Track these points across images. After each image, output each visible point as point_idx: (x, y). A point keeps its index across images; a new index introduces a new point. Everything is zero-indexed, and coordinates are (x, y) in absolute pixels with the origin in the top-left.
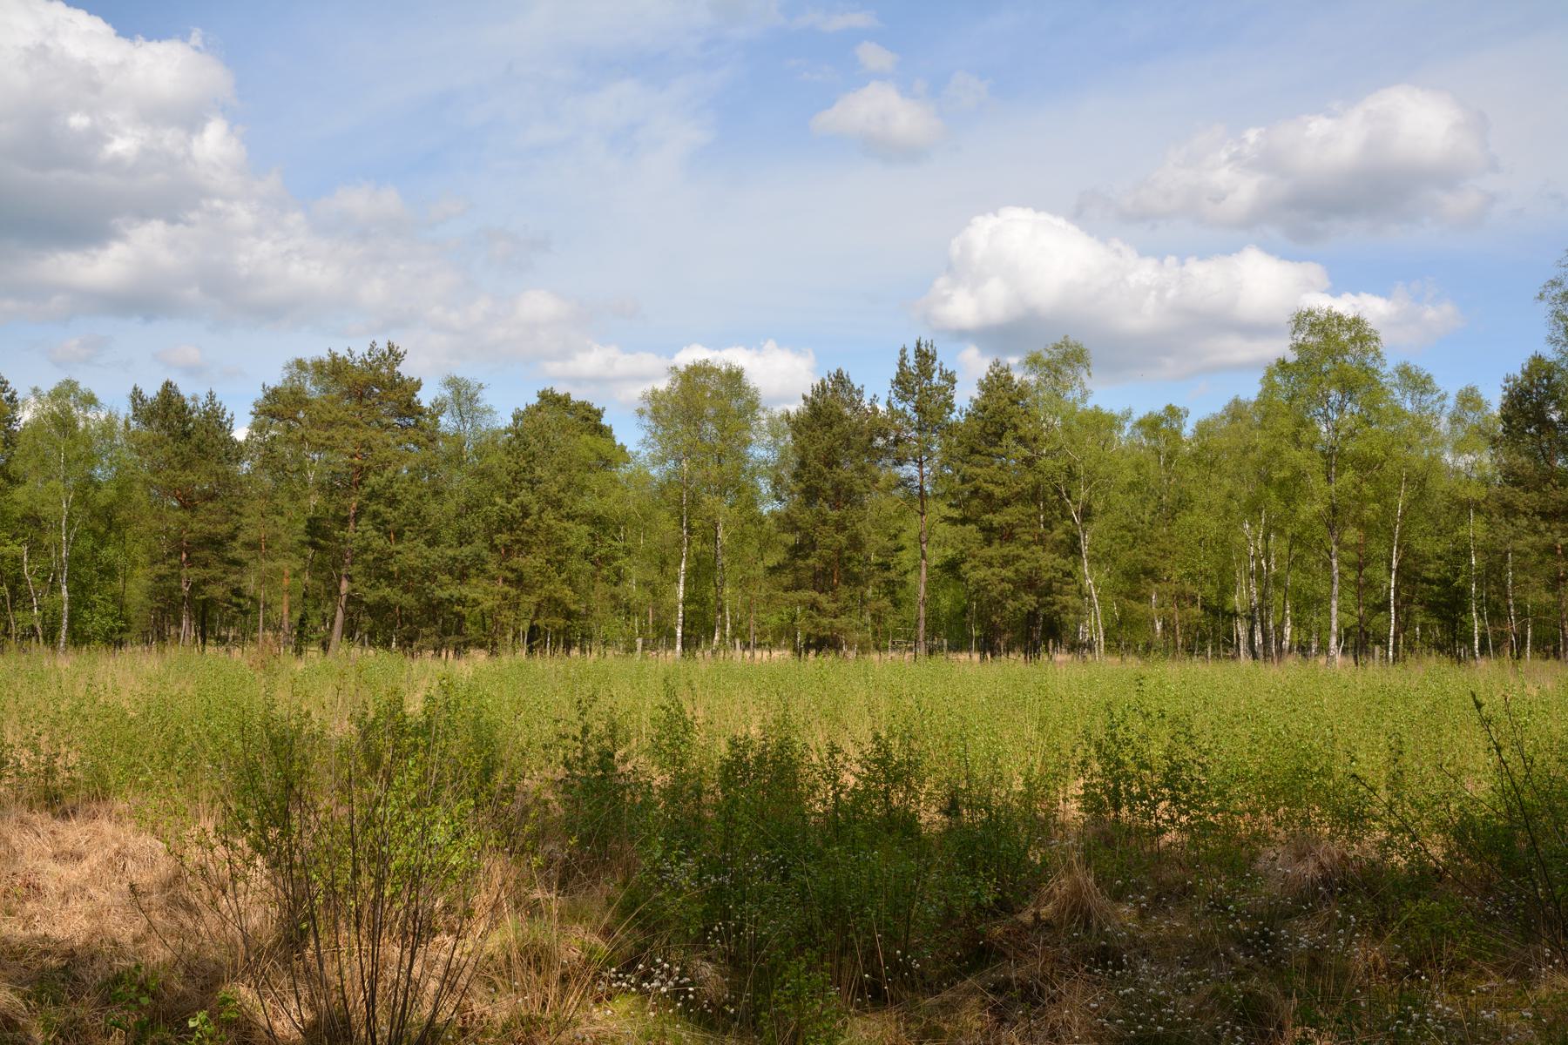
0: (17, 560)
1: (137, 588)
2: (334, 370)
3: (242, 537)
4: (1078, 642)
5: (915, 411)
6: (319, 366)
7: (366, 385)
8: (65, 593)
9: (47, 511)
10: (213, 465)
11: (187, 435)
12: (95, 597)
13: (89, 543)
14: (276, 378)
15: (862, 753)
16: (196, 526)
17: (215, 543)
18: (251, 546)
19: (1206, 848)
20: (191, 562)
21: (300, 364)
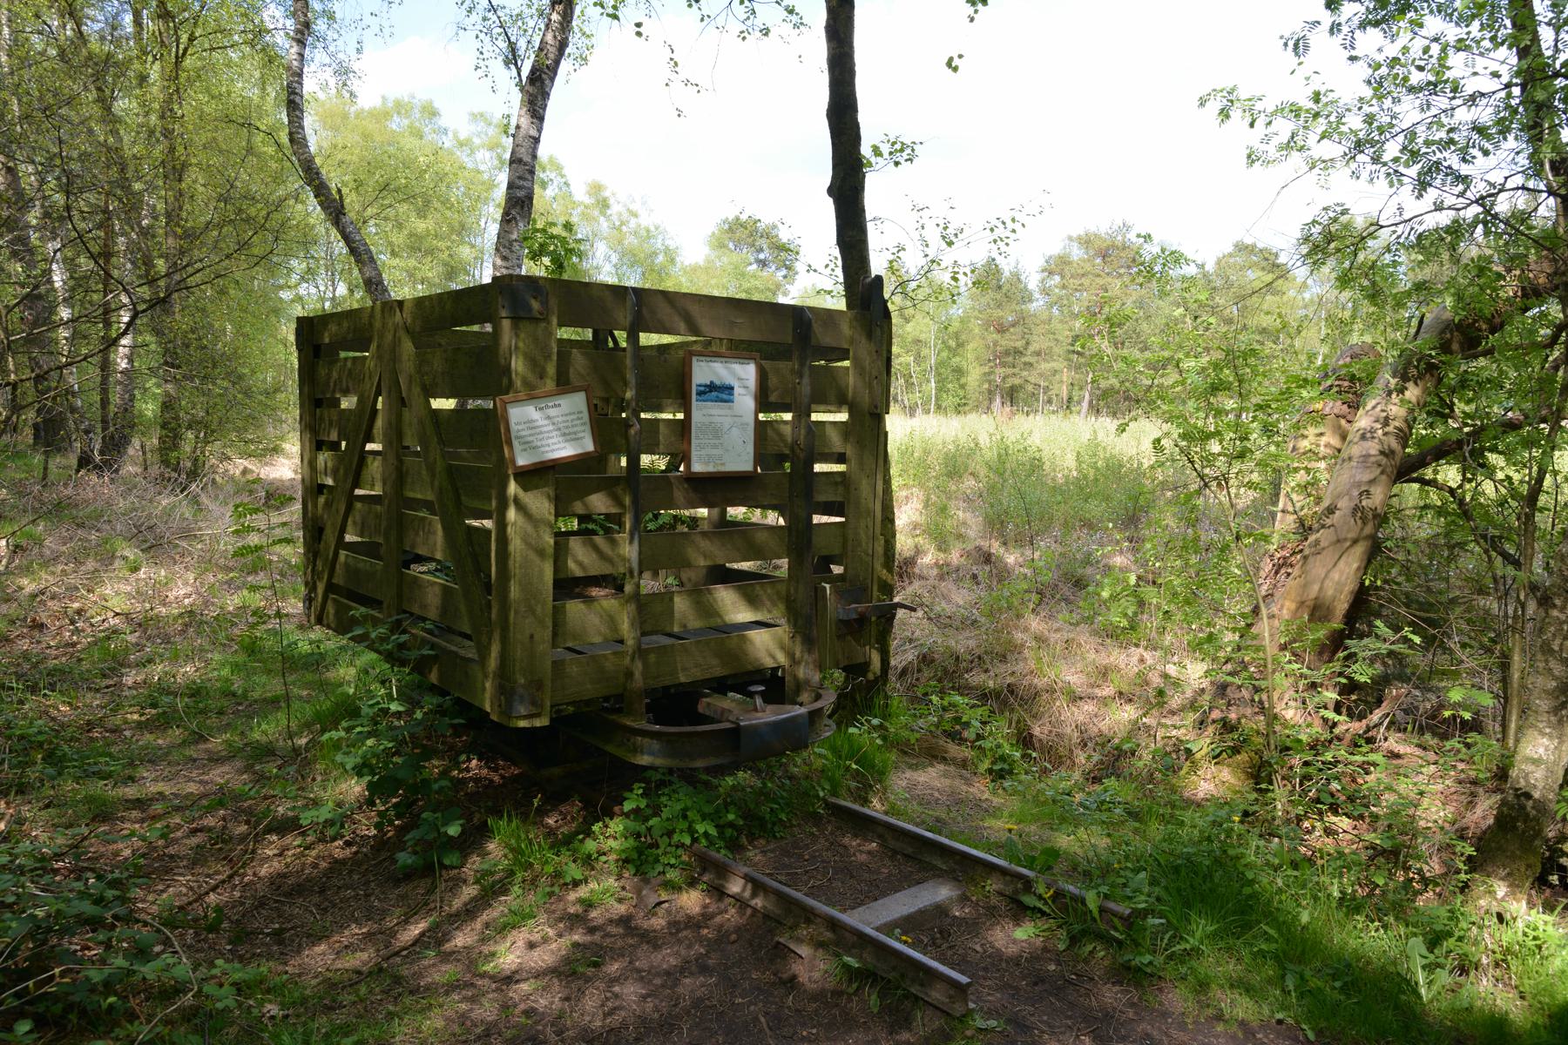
0: (909, 364)
1: (974, 376)
2: (1086, 241)
3: (1031, 348)
4: (1414, 297)
5: (425, 217)
6: (1079, 238)
7: (1108, 249)
8: (933, 385)
9: (923, 337)
10: (1014, 306)
11: (1000, 287)
12: (950, 386)
13: (945, 354)
14: (1056, 249)
15: (1446, 81)
16: (1003, 343)
17: (1018, 352)
18: (1038, 354)
19: (1395, 264)
20: (1004, 365)
21: (1070, 238)
